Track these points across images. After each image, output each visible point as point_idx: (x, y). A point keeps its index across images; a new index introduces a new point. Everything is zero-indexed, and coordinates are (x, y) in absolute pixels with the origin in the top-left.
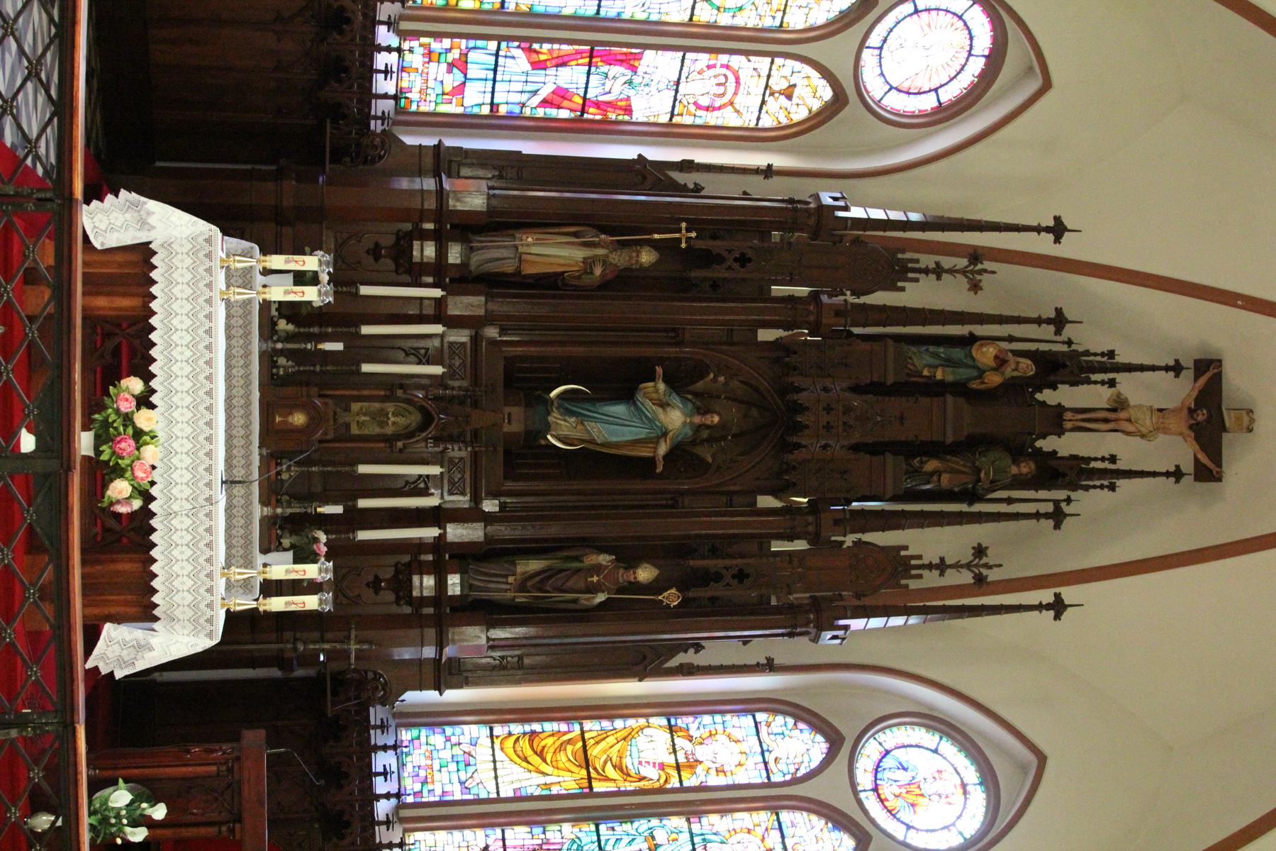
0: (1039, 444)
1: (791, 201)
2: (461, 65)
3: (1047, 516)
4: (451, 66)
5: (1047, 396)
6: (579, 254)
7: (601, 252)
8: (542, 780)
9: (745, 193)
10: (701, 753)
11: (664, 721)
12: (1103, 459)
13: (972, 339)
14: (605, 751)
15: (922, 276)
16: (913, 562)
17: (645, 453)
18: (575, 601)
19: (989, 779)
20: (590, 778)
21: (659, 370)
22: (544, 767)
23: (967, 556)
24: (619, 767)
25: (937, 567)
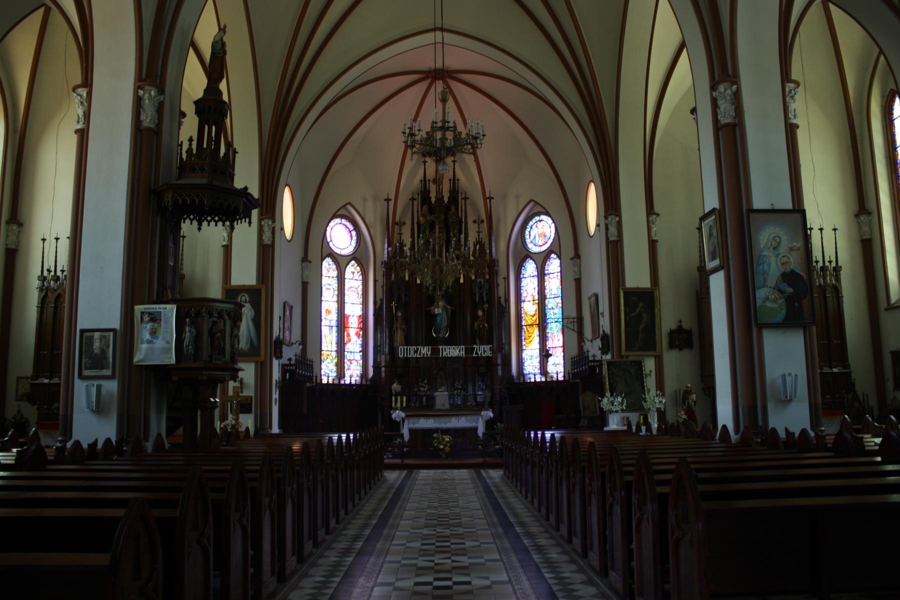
0: (446, 202)
1: (383, 275)
2: (350, 361)
3: (465, 202)
4: (351, 363)
5: (433, 200)
6: (399, 332)
7: (398, 326)
8: (536, 337)
9: (382, 287)
10: (530, 294)
11: (522, 303)
12: (450, 183)
13: (418, 223)
14: (529, 320)
15: (402, 239)
16: (478, 240)
17: (450, 311)
18: (487, 331)
19: (539, 214)
20: (536, 324)
21: (428, 309)
22: (533, 337)
23: (476, 225)
24: (533, 316)
25: (479, 234)
